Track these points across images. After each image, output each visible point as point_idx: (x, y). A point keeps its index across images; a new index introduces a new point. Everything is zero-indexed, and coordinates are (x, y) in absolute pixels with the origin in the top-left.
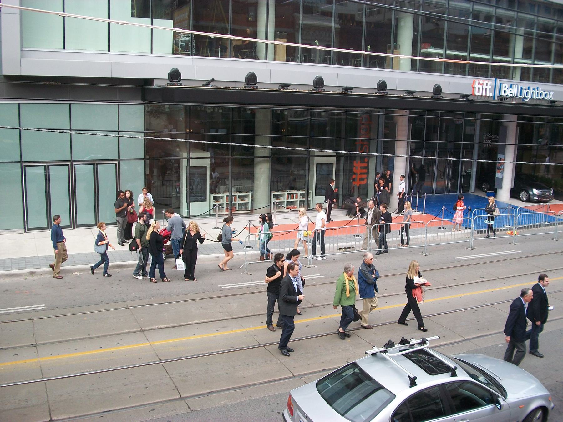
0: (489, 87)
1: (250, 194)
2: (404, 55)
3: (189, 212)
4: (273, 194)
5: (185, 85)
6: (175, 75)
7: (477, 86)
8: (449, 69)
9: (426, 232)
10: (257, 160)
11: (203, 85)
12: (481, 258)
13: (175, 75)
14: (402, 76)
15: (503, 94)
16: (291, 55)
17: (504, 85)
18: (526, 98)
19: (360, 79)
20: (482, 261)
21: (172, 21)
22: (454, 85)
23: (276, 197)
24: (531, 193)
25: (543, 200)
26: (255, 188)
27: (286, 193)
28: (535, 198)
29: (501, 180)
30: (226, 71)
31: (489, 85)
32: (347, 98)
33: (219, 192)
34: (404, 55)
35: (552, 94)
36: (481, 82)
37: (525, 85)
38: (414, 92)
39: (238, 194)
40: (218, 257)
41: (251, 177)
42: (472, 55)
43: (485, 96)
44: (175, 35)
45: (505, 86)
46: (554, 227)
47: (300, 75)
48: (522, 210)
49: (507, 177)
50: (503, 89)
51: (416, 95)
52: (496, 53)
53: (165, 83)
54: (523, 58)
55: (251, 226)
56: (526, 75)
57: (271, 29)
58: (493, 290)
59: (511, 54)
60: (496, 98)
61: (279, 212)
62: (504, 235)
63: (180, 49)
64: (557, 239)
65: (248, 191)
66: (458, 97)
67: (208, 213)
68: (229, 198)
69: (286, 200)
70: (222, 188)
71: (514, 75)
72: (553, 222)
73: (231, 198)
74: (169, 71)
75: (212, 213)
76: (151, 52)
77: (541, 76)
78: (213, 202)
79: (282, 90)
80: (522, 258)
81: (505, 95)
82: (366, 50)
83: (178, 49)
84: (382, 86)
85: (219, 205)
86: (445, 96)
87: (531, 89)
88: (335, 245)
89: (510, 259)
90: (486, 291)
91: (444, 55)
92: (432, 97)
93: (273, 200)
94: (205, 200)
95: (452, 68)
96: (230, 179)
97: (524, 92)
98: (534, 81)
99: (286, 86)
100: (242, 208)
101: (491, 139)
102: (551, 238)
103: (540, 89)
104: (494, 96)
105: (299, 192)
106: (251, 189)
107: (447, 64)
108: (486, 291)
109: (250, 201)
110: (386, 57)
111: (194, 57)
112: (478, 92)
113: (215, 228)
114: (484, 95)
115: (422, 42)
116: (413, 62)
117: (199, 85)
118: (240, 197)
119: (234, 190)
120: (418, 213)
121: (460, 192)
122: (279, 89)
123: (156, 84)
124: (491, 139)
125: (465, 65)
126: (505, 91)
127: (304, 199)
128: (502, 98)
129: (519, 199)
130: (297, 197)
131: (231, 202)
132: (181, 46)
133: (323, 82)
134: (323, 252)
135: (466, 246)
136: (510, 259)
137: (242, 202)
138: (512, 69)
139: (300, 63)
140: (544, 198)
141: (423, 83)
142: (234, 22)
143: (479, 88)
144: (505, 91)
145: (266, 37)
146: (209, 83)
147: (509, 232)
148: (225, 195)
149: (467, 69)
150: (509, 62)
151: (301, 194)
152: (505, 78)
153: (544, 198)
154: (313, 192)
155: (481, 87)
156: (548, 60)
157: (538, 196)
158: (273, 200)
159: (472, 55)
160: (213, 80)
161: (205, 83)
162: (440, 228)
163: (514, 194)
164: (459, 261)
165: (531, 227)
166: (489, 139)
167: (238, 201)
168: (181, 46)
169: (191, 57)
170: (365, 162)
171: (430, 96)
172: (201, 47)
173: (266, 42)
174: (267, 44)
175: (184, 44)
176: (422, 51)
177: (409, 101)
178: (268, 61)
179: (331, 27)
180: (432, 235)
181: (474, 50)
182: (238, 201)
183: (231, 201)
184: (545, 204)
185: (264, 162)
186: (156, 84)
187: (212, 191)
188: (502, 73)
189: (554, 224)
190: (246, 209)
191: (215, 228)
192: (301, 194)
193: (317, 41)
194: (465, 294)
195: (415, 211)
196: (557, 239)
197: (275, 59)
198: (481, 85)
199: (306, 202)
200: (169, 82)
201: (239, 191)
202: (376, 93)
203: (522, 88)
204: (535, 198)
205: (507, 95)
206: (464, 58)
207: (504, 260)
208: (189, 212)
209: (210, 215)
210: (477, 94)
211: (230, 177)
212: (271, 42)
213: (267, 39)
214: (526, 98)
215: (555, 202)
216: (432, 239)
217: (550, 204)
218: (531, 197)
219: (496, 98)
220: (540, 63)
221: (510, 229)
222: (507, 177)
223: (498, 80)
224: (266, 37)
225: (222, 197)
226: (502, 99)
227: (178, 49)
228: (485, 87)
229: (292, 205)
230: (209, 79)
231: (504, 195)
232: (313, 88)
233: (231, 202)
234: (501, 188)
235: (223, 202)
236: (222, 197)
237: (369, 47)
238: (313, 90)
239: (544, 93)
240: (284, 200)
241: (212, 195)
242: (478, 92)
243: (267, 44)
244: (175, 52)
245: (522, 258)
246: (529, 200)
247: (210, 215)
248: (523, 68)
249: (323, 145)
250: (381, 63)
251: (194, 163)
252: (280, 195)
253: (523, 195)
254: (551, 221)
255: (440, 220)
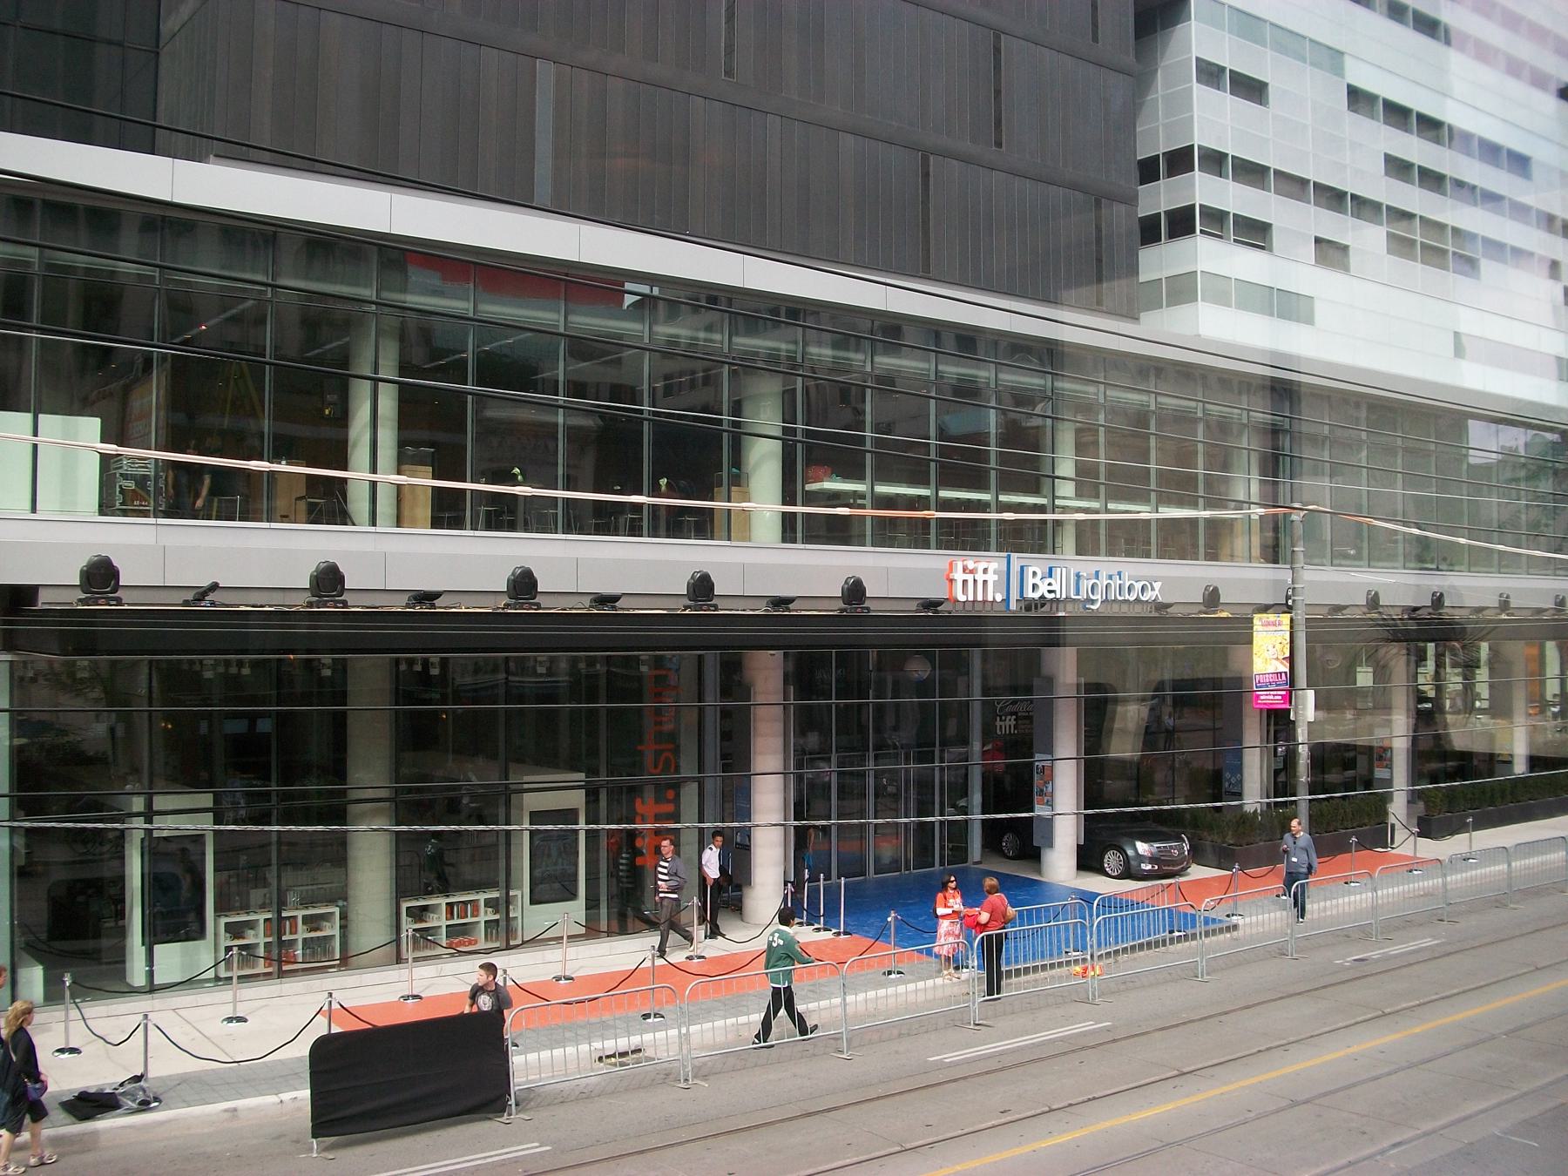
0: (991, 578)
1: (337, 910)
2: (762, 499)
3: (151, 974)
4: (404, 906)
5: (130, 602)
6: (101, 575)
7: (959, 576)
8: (887, 534)
9: (845, 989)
10: (353, 809)
11: (186, 603)
12: (1002, 1053)
13: (101, 575)
14: (758, 556)
15: (1030, 594)
16: (447, 512)
17: (1031, 570)
18: (1093, 602)
19: (638, 569)
20: (1007, 1061)
21: (98, 421)
22: (898, 575)
23: (419, 914)
24: (1130, 852)
25: (1165, 869)
26: (351, 893)
27: (442, 901)
28: (1143, 866)
29: (1049, 823)
30: (255, 559)
31: (990, 571)
32: (606, 626)
33: (245, 908)
34: (762, 499)
35: (1157, 585)
36: (971, 565)
37: (1087, 565)
38: (790, 600)
39: (300, 914)
40: (235, 1110)
41: (337, 854)
42: (944, 494)
43: (984, 602)
44: (105, 459)
45: (1035, 574)
46: (1194, 943)
47: (469, 565)
48: (1110, 903)
49: (1063, 810)
50: (1030, 581)
51: (796, 609)
52: (1007, 484)
53: (73, 599)
54: (1079, 495)
55: (335, 1006)
56: (1088, 540)
57: (388, 437)
58: (1036, 1146)
59: (1046, 489)
60: (1013, 606)
61: (426, 958)
62: (1068, 977)
63: (119, 499)
64: (1206, 978)
65: (331, 901)
66: (913, 606)
67: (211, 974)
68: (275, 923)
69: (444, 923)
70: (256, 895)
71: (1058, 540)
72: (1190, 932)
73: (278, 926)
74: (83, 563)
75: (223, 974)
76: (34, 510)
77: (1129, 540)
78: (225, 941)
79: (418, 609)
80: (1114, 1041)
81: (1036, 595)
82: (655, 491)
83: (119, 495)
84: (702, 587)
85: (241, 947)
86: (876, 608)
87: (1103, 575)
88: (584, 1048)
89: (1083, 1049)
90: (1018, 1151)
91: (869, 496)
92: (842, 610)
93: (408, 926)
94: (200, 934)
95: (891, 534)
96: (274, 868)
97: (1086, 585)
98: (1111, 553)
99: (428, 597)
100: (313, 954)
101: (1015, 713)
102: (1191, 973)
103: (1126, 575)
104: (1006, 601)
105: (481, 897)
106: (340, 896)
107: (880, 522)
108: (1018, 1151)
109: (336, 932)
110: (712, 510)
111: (161, 521)
112: (965, 590)
113: (230, 1020)
114: (980, 598)
115: (809, 462)
116: (788, 522)
117: (174, 602)
118: (306, 919)
119: (292, 898)
120: (828, 935)
121: (942, 864)
122: (408, 606)
123: (44, 600)
124: (1015, 713)
125: (926, 522)
126: (1035, 587)
127: (497, 917)
128: (1029, 605)
129: (1101, 871)
130: (475, 913)
131: (279, 938)
132: (122, 491)
133: (534, 583)
134: (1520, 163)
135: (954, 1020)
136: (1083, 1049)
137: (313, 934)
138: (1050, 525)
139: (471, 533)
140: (1168, 863)
141: (816, 574)
142: (280, 414)
143: (965, 582)
144: (1035, 587)
145: (373, 464)
146: (202, 594)
147: (1078, 969)
148: (261, 917)
149: (933, 531)
150: (1041, 509)
151: (488, 903)
152: (1041, 549)
153: (1168, 863)
154: (522, 893)
155: (970, 577)
156: (1140, 497)
157: (1152, 860)
158: (408, 926)
159: (944, 494)
160: (214, 587)
161: (190, 596)
162: (890, 973)
163: (1088, 860)
164: (941, 1066)
165: (1141, 946)
166: (1011, 714)
167: (302, 934)
168: (122, 491)
169: (152, 520)
170: (669, 801)
171: (834, 608)
172: (182, 496)
173: (373, 477)
174: (374, 484)
175: (131, 485)
176: (808, 487)
177: (779, 623)
178: (378, 529)
179: (556, 425)
180: (861, 997)
181: (944, 482)
182: (302, 934)
183: (280, 933)
184: (1165, 882)
185: (375, 814)
186: (44, 600)
187: (221, 909)
188: (1029, 538)
189: (1194, 937)
190: (327, 952)
191: (230, 1020)
192: (488, 903)
193: (517, 470)
194: (958, 1168)
195: (818, 930)
196: (1206, 978)
197: (399, 523)
198: (971, 572)
199: (503, 924)
200: (83, 596)
201: (306, 902)
202: (686, 608)
203: (1078, 576)
204: (1143, 866)
205: (1042, 597)
206: (921, 503)
207: (1065, 1053)
208: (151, 974)
209: (217, 979)
210: (962, 598)
211: (274, 861)
212: (388, 477)
213: (374, 470)
214: (1093, 602)
215: (1197, 872)
216: (861, 1008)
217: (1182, 879)
218: (1133, 863)
219: (1013, 606)
220: (1122, 507)
221: (1076, 962)
222: (1063, 810)
223: (1014, 556)
224: (373, 464)
225: (251, 925)
226: (1028, 609)
227: (119, 495)
228: (980, 577)
229: (464, 933)
230: (206, 583)
231: (1060, 864)
232: (505, 600)
233: (279, 938)
234: (1051, 845)
235: (258, 938)
236: (251, 925)
237: (663, 481)
238: (507, 606)
239: (1138, 586)
240: (439, 920)
241: (223, 920)
242: (965, 590)
243: (374, 484)
244: (105, 508)
245: (1114, 1041)
246: (1128, 873)
247: (217, 979)
248: (1078, 523)
249: (548, 759)
250: (701, 526)
251: (166, 826)
252: (425, 908)
253: (1111, 860)
254: (1182, 926)
255: (889, 951)
